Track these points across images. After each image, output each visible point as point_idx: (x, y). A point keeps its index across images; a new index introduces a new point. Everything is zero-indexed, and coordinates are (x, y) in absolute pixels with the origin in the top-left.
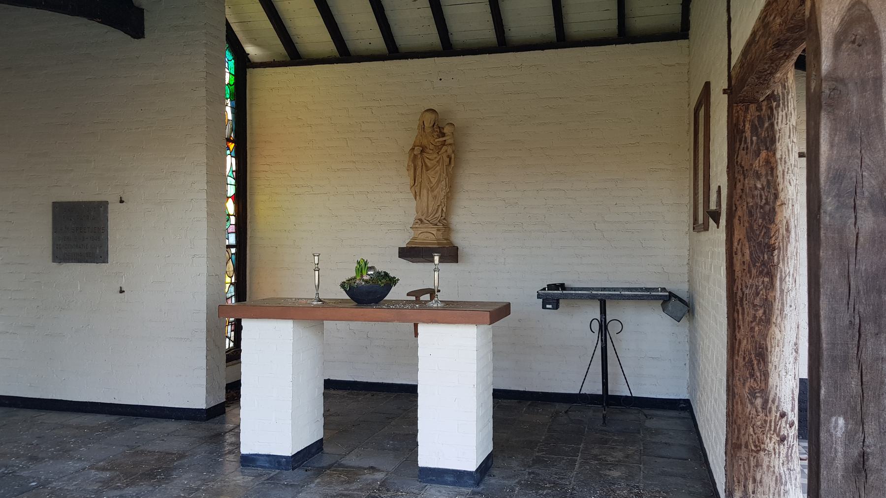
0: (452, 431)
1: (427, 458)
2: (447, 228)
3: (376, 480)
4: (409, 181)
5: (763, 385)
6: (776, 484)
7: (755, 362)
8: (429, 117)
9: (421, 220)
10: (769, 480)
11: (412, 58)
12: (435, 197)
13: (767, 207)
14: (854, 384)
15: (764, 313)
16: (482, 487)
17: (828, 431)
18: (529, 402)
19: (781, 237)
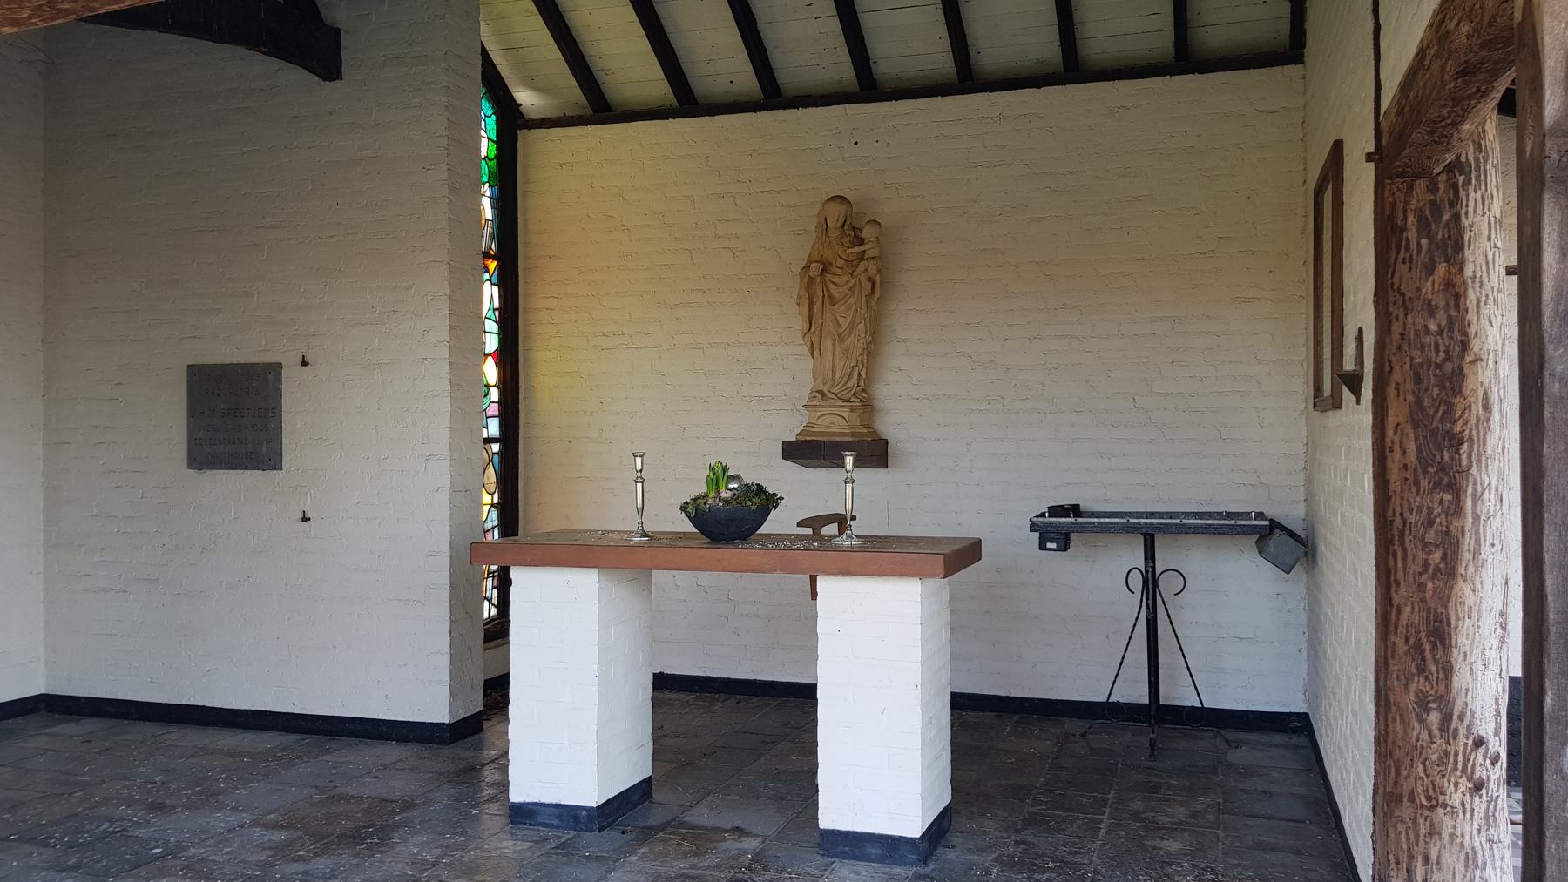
0: (879, 767)
1: (834, 814)
2: (868, 407)
3: (743, 852)
4: (800, 323)
5: (1442, 689)
6: (1466, 867)
7: (1427, 647)
8: (837, 210)
11: (805, 106)
12: (846, 352)
15: (1444, 557)
16: (932, 866)
18: (1016, 718)
19: (1473, 421)
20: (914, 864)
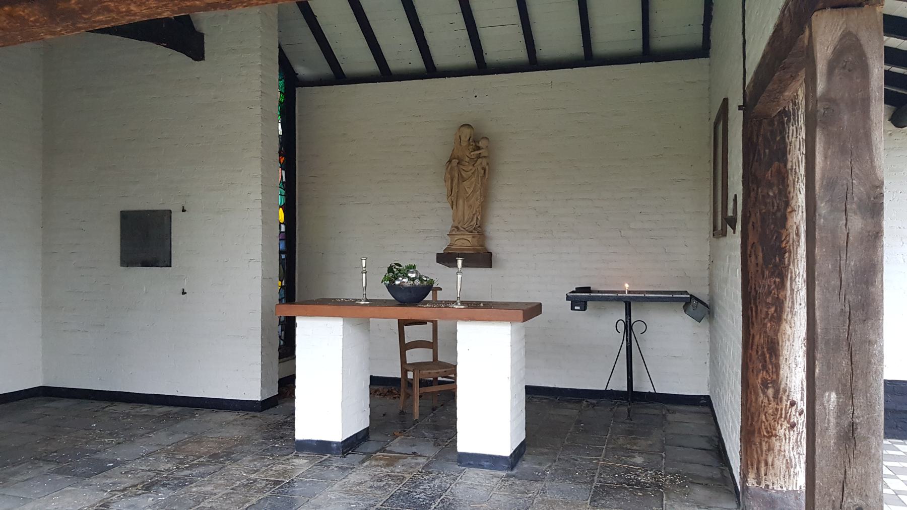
0: (488, 417)
1: (465, 444)
4: (445, 191)
5: (775, 377)
7: (768, 356)
8: (467, 132)
9: (457, 228)
10: (780, 464)
11: (449, 77)
13: (779, 214)
14: (845, 362)
15: (776, 311)
16: (515, 471)
17: (822, 404)
19: (791, 242)
20: (508, 469)
